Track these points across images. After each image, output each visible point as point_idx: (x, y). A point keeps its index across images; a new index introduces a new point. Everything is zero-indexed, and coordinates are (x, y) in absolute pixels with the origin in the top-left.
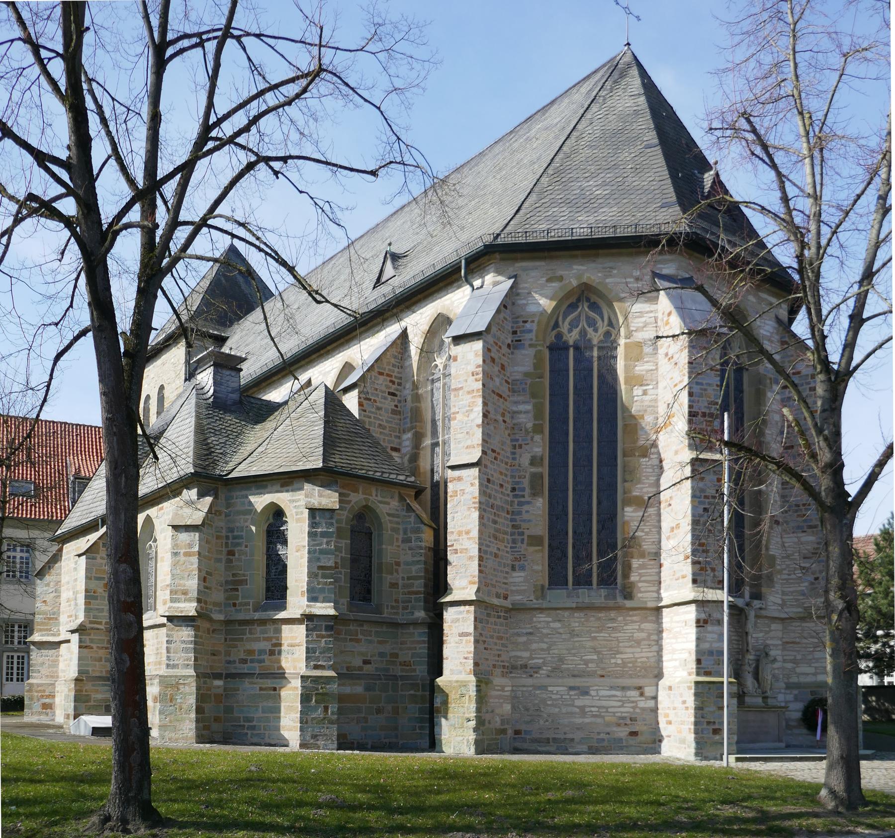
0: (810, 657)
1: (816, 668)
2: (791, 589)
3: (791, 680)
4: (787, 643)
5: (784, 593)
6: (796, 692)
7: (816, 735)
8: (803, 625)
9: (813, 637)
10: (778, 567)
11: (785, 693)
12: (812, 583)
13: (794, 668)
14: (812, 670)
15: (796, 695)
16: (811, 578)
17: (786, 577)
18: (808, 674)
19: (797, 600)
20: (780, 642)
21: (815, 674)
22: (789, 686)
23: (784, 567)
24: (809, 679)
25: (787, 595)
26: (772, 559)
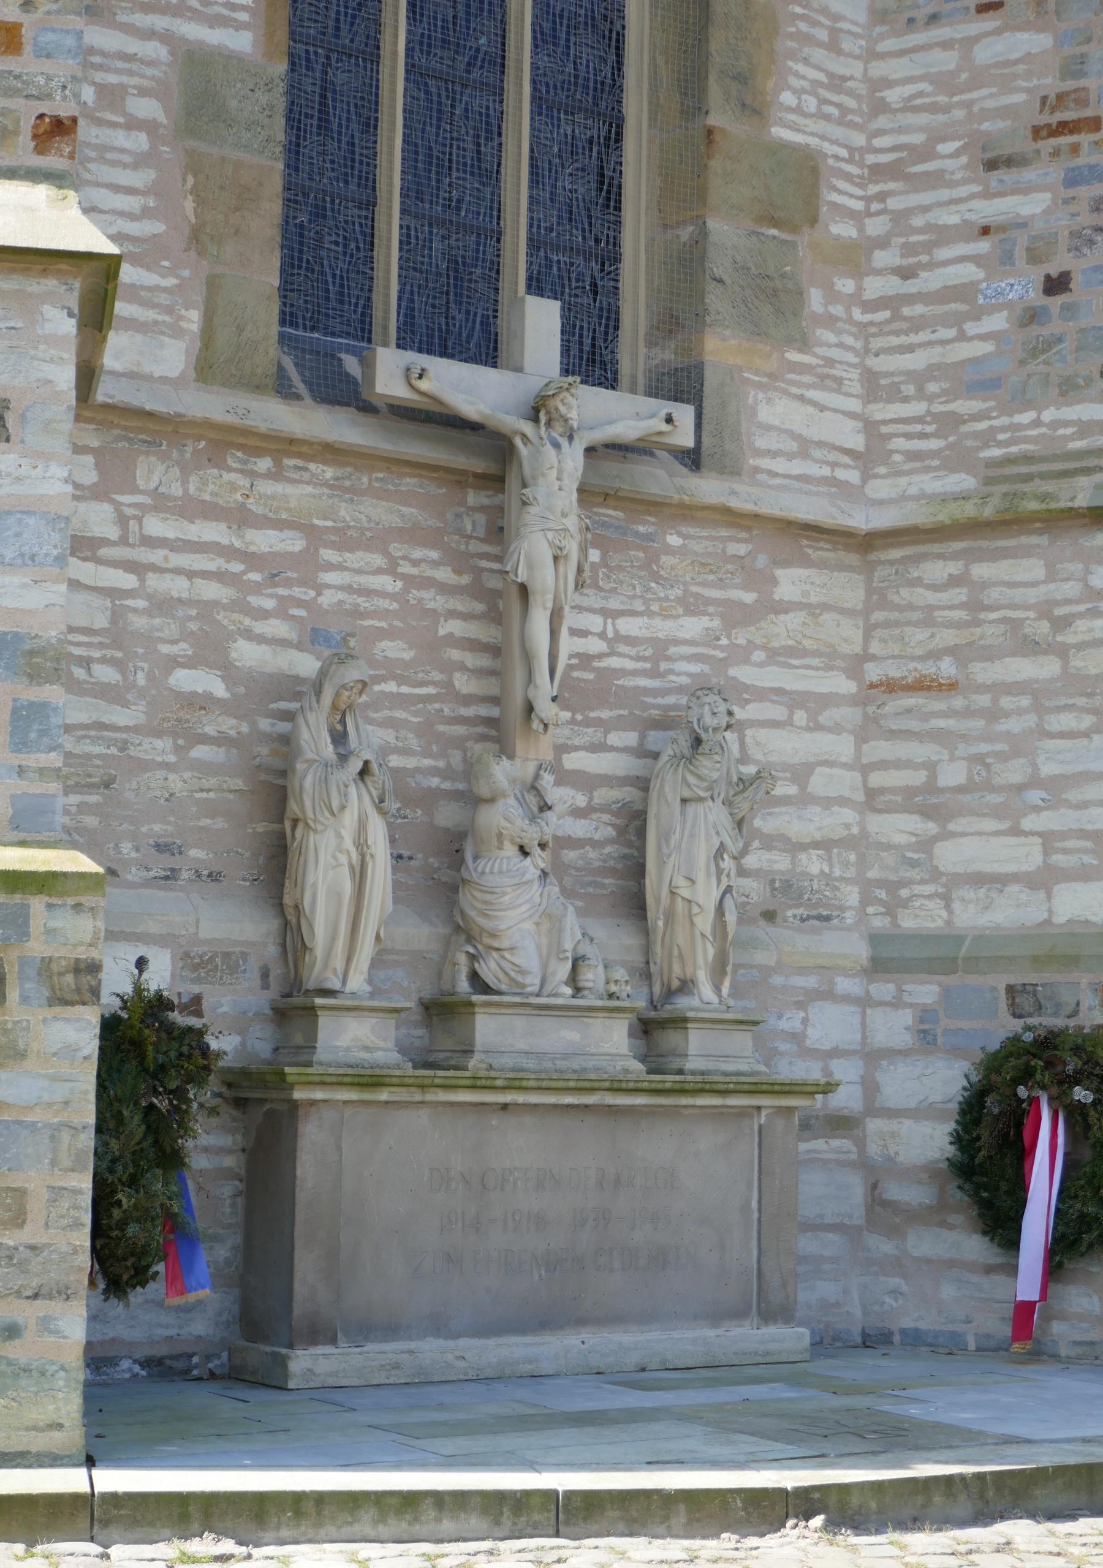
0: (1014, 772)
1: (1048, 839)
2: (916, 361)
3: (908, 922)
4: (891, 687)
5: (874, 387)
6: (925, 992)
7: (1012, 1270)
8: (981, 571)
9: (1031, 647)
10: (844, 230)
11: (865, 1002)
12: (1032, 316)
13: (926, 845)
14: (1027, 856)
15: (925, 1015)
16: (1022, 286)
17: (892, 285)
18: (1000, 881)
19: (950, 422)
20: (848, 687)
21: (1042, 881)
22: (889, 959)
23: (876, 227)
24: (1011, 912)
25: (895, 395)
26: (805, 171)
